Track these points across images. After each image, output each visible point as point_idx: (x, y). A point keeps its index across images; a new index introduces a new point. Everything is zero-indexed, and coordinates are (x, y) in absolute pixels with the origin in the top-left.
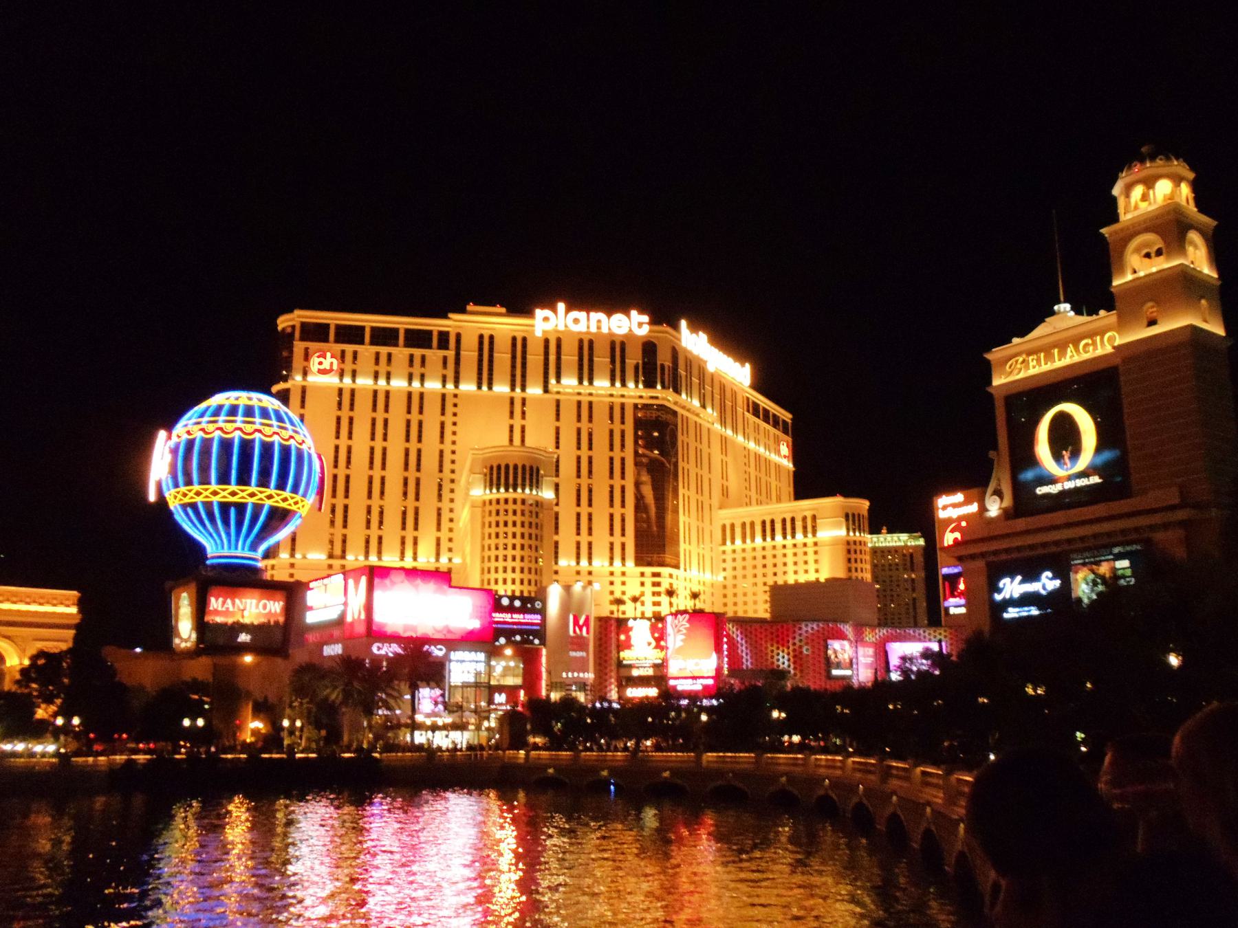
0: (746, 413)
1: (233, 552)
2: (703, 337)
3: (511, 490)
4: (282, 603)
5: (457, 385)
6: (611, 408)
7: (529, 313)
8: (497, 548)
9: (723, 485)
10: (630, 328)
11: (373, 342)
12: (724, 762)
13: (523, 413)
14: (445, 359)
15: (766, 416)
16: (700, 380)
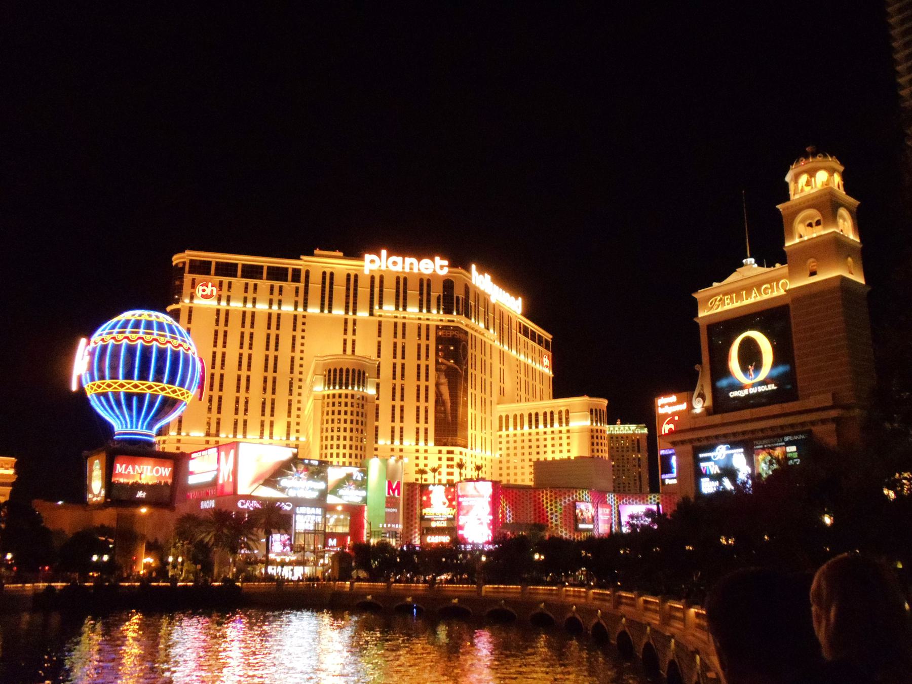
0: (518, 333)
1: (134, 430)
2: (488, 277)
3: (344, 388)
4: (170, 469)
5: (305, 310)
6: (419, 328)
11: (244, 276)
13: (354, 331)
14: (297, 289)
15: (533, 336)
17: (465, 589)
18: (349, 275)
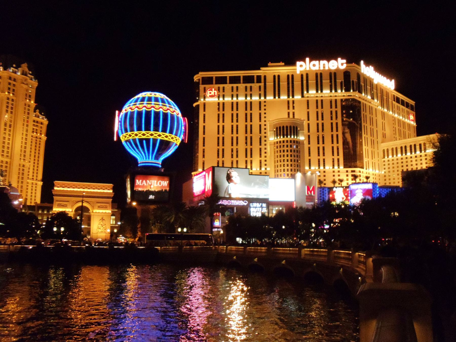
0: (393, 102)
1: (147, 161)
2: (371, 68)
3: (285, 137)
4: (168, 182)
5: (265, 98)
6: (331, 102)
7: (294, 64)
8: (281, 161)
9: (383, 133)
10: (338, 66)
11: (231, 83)
12: (313, 255)
13: (293, 107)
14: (260, 87)
15: (403, 103)
16: (371, 87)
17: (291, 252)
18: (288, 76)
